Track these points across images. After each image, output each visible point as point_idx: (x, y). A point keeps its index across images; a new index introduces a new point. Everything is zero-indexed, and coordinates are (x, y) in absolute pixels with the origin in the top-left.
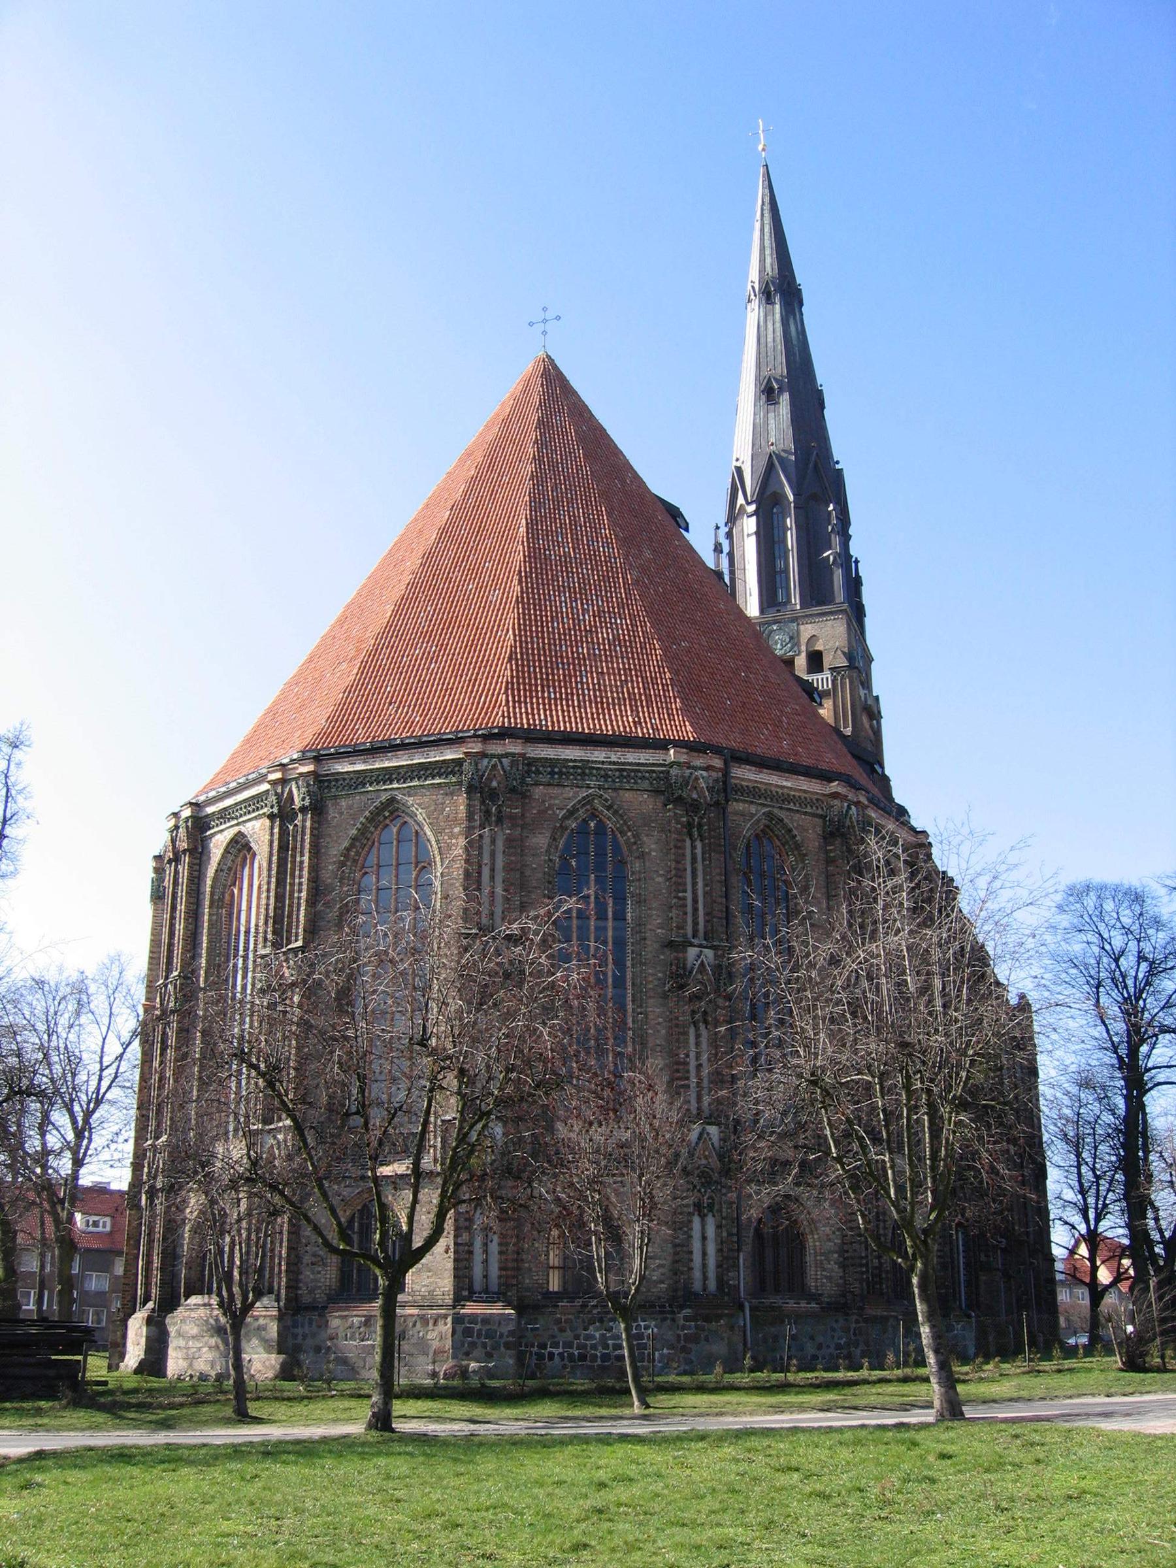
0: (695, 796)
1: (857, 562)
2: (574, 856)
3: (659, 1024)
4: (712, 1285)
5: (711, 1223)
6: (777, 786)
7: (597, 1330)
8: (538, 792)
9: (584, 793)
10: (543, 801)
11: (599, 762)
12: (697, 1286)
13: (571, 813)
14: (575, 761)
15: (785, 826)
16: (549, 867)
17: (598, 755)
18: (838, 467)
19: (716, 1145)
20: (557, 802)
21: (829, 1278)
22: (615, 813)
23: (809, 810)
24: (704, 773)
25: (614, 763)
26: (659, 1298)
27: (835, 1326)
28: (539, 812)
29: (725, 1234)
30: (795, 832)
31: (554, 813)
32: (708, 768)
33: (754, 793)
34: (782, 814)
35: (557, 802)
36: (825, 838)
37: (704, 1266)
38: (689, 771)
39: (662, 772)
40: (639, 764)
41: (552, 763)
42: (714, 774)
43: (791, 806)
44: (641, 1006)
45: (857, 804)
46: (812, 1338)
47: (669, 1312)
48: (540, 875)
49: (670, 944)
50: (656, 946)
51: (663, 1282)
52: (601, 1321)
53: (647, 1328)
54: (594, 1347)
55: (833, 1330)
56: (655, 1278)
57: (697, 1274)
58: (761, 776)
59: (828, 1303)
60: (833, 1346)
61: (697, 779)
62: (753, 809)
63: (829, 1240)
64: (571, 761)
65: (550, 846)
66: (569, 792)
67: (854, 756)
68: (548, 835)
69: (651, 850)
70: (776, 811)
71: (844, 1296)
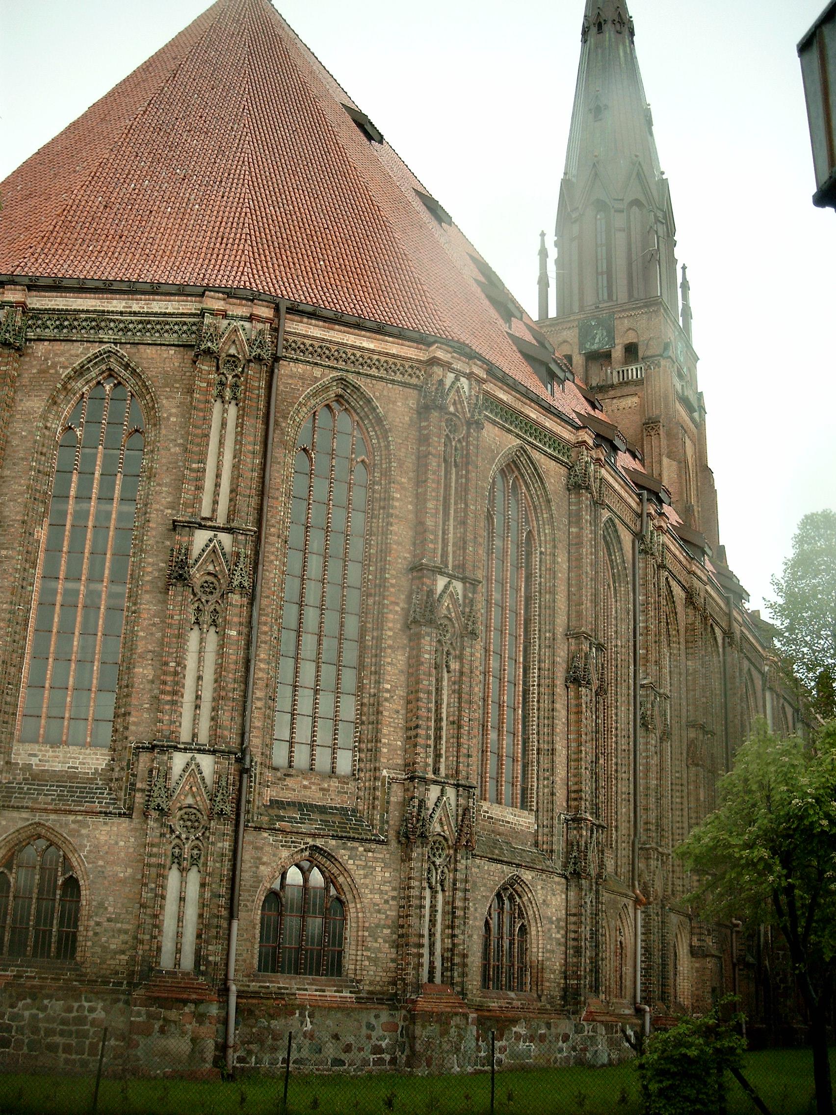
0: (232, 351)
1: (684, 268)
2: (81, 425)
3: (154, 625)
4: (188, 962)
5: (193, 878)
6: (353, 347)
7: (26, 1007)
8: (41, 348)
9: (96, 349)
10: (46, 360)
11: (117, 312)
12: (166, 962)
13: (80, 372)
14: (88, 311)
15: (363, 396)
16: (43, 436)
17: (117, 304)
18: (664, 177)
19: (209, 781)
20: (62, 359)
21: (375, 961)
22: (134, 372)
23: (398, 377)
24: (247, 325)
25: (135, 313)
26: (117, 973)
27: (373, 1021)
28: (40, 372)
29: (207, 895)
30: (376, 403)
31: (57, 372)
32: (251, 318)
33: (321, 353)
34: (360, 382)
35: (62, 359)
36: (419, 413)
37: (179, 935)
38: (226, 322)
39: (194, 324)
40: (165, 314)
41: (61, 314)
42: (260, 326)
43: (374, 372)
44: (135, 604)
45: (470, 376)
46: (336, 1037)
47: (123, 992)
48: (29, 444)
49: (175, 526)
50: (162, 529)
51: (123, 952)
52: (34, 997)
53: (92, 1010)
54: (20, 1030)
55: (370, 1027)
56: (113, 947)
57: (168, 946)
58: (332, 333)
59: (370, 992)
60: (368, 1048)
61: (236, 331)
62: (317, 372)
63: (379, 911)
64: (83, 311)
65: (48, 410)
66: (78, 348)
67: (520, 352)
68: (46, 397)
69: (170, 415)
70: (351, 377)
71: (394, 983)
